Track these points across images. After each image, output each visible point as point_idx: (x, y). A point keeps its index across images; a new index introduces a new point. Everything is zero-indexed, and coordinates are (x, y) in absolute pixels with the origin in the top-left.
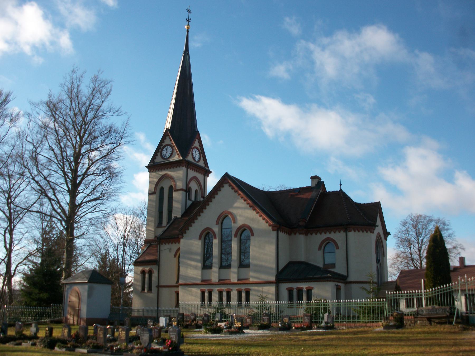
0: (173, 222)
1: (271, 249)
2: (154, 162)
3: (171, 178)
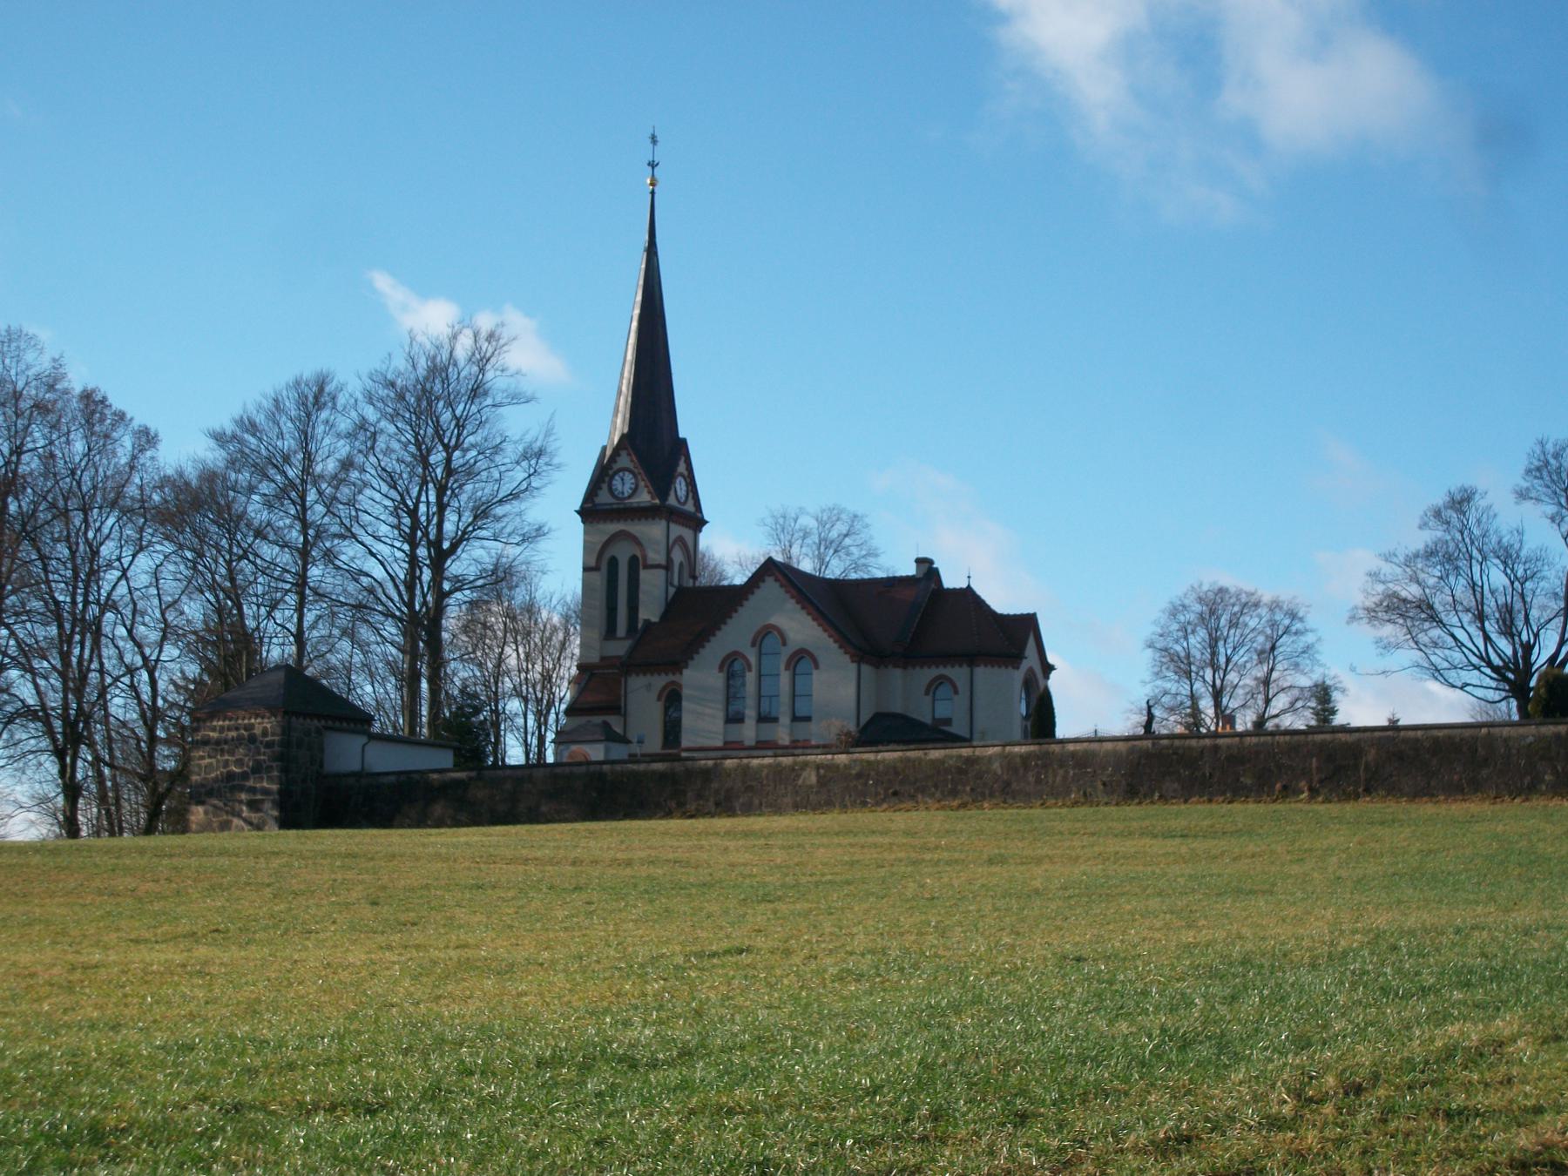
0: (642, 634)
1: (847, 692)
2: (593, 501)
3: (635, 540)
